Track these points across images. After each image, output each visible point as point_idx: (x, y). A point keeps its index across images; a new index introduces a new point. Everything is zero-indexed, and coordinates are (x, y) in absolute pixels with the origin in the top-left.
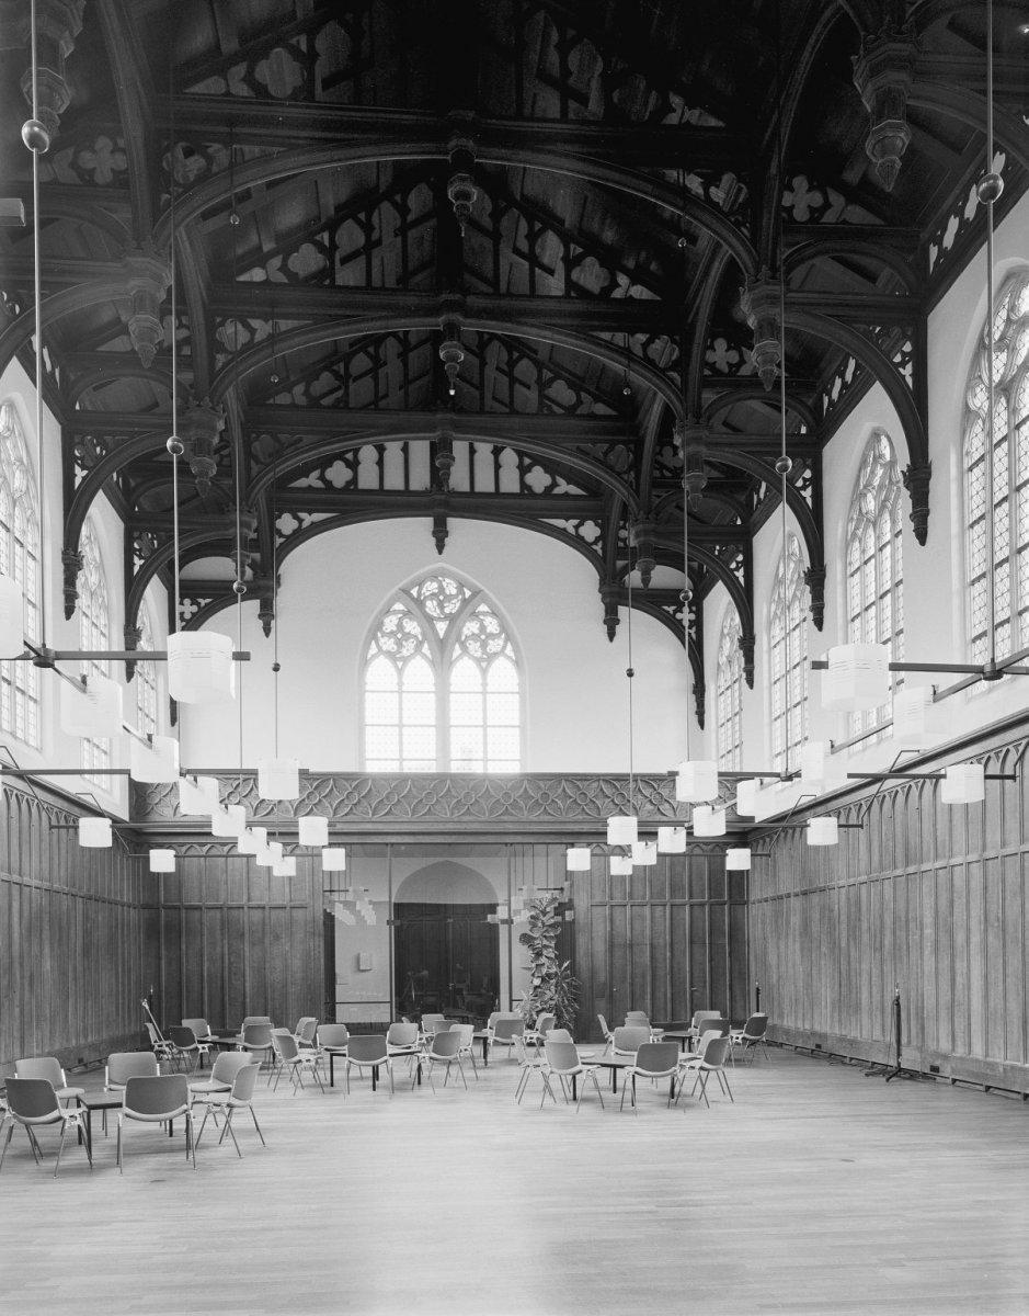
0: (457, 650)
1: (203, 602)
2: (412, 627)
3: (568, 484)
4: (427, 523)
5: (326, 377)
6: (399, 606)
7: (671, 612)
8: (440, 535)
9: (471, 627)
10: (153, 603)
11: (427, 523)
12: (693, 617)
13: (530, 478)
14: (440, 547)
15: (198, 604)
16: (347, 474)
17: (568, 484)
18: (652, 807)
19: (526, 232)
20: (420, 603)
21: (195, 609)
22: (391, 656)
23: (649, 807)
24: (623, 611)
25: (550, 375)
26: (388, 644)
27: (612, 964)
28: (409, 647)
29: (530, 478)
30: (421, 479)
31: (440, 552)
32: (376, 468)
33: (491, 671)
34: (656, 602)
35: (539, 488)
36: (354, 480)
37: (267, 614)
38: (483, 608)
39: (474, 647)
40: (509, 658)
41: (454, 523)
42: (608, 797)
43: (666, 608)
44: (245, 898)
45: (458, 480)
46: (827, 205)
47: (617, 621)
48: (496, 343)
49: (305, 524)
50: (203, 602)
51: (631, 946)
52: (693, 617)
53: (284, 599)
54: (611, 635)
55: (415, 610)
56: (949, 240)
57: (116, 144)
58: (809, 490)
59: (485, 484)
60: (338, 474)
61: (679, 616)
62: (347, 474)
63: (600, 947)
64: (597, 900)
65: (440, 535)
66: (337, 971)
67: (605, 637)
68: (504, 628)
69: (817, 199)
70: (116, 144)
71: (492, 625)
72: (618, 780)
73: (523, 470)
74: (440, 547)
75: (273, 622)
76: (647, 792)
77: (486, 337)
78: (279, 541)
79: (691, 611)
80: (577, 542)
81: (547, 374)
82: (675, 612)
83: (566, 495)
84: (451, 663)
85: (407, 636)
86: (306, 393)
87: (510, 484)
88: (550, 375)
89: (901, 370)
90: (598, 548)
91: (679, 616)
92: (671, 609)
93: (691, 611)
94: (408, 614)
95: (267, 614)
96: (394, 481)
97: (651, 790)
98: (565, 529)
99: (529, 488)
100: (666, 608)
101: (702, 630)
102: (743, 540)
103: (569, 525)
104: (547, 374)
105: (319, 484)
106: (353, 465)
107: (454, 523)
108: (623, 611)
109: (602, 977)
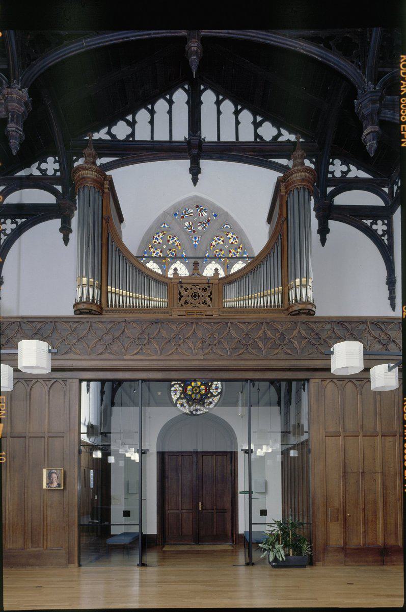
1: (19, 221)
4: (186, 163)
7: (369, 225)
8: (195, 172)
11: (186, 163)
12: (385, 228)
13: (260, 131)
14: (195, 181)
16: (129, 130)
18: (381, 347)
24: (332, 224)
27: (345, 492)
29: (260, 131)
30: (181, 133)
31: (195, 185)
32: (149, 126)
35: (268, 138)
36: (133, 134)
41: (204, 164)
43: (365, 221)
45: (208, 133)
46: (349, 170)
47: (328, 231)
51: (363, 473)
52: (385, 228)
57: (55, 159)
58: (386, 236)
59: (228, 136)
60: (121, 130)
61: (374, 227)
62: (129, 130)
63: (335, 476)
64: (332, 429)
65: (195, 172)
66: (112, 493)
69: (345, 168)
70: (55, 159)
73: (257, 125)
74: (195, 181)
76: (376, 333)
82: (372, 224)
87: (247, 135)
89: (382, 237)
91: (374, 227)
92: (369, 222)
93: (384, 224)
96: (161, 135)
99: (261, 137)
100: (365, 221)
101: (393, 237)
105: (108, 138)
106: (132, 124)
107: (204, 164)
108: (332, 224)
109: (336, 502)
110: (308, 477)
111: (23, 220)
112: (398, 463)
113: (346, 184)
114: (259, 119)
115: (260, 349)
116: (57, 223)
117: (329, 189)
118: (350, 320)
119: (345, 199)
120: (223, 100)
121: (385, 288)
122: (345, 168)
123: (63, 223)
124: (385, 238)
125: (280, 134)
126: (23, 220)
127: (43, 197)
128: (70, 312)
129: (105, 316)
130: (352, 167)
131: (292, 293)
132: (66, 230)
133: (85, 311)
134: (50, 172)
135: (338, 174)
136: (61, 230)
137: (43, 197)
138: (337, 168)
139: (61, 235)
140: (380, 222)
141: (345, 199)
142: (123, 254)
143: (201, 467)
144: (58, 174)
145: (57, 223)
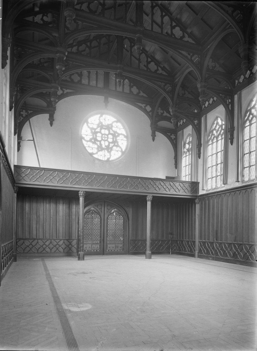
1: (30, 112)
3: (66, 90)
5: (84, 46)
10: (237, 98)
12: (175, 137)
17: (66, 90)
19: (163, 25)
25: (150, 60)
34: (166, 132)
37: (52, 120)
48: (127, 40)
49: (65, 92)
50: (30, 112)
52: (175, 137)
53: (56, 115)
56: (241, 80)
61: (171, 136)
69: (162, 112)
75: (53, 122)
77: (124, 37)
79: (174, 136)
80: (145, 111)
81: (149, 60)
83: (142, 96)
86: (78, 49)
88: (150, 60)
90: (151, 113)
92: (169, 134)
93: (174, 136)
95: (52, 120)
98: (142, 107)
102: (203, 112)
103: (143, 106)
104: (149, 60)
112: (4, 131)
114: (132, 84)
120: (165, 16)
121: (174, 160)
122: (162, 112)
123: (50, 116)
124: (174, 141)
128: (165, 178)
129: (200, 180)
130: (165, 112)
133: (190, 161)
139: (49, 122)
140: (173, 135)
143: (95, 207)
145: (47, 116)
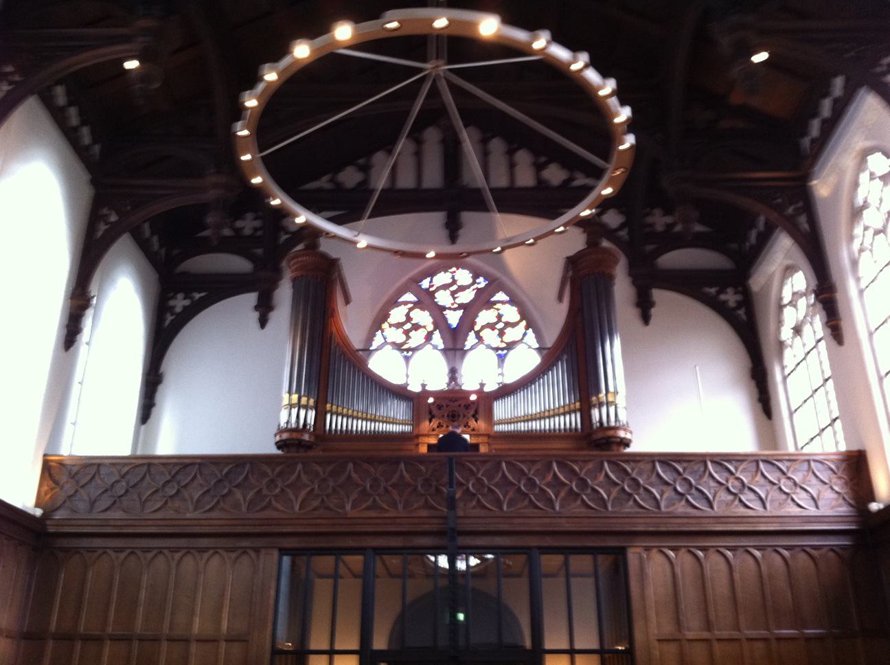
0: (471, 339)
1: (197, 296)
2: (423, 317)
6: (409, 297)
9: (485, 317)
12: (739, 297)
15: (191, 298)
20: (430, 294)
21: (187, 302)
22: (398, 347)
23: (723, 496)
26: (397, 336)
28: (417, 338)
30: (433, 178)
33: (412, 361)
38: (501, 296)
39: (487, 335)
40: (435, 347)
42: (667, 483)
44: (166, 625)
50: (197, 296)
54: (263, 322)
55: (426, 299)
61: (723, 297)
67: (256, 325)
68: (524, 315)
71: (511, 313)
72: (679, 462)
73: (539, 167)
78: (284, 237)
84: (465, 352)
85: (416, 327)
91: (723, 297)
92: (713, 290)
94: (417, 305)
97: (726, 474)
108: (658, 295)
110: (324, 555)
111: (202, 294)
113: (672, 241)
115: (550, 500)
116: (251, 298)
117: (650, 248)
118: (680, 458)
119: (675, 259)
121: (878, 278)
124: (741, 312)
125: (571, 179)
126: (202, 294)
127: (237, 264)
131: (595, 413)
132: (265, 309)
134: (247, 232)
135: (660, 228)
136: (257, 308)
137: (237, 264)
138: (659, 221)
139: (256, 315)
141: (675, 259)
142: (359, 368)
144: (259, 233)
145: (251, 298)
